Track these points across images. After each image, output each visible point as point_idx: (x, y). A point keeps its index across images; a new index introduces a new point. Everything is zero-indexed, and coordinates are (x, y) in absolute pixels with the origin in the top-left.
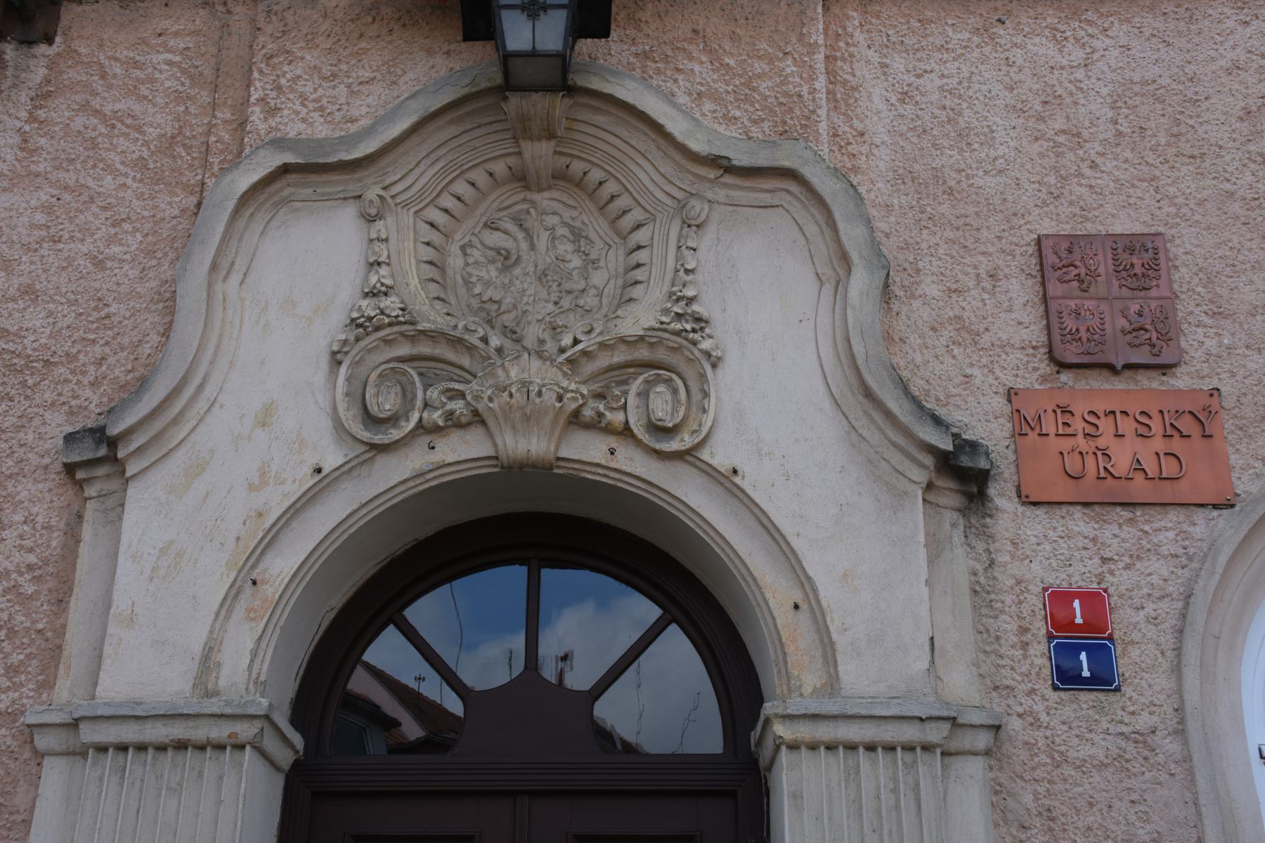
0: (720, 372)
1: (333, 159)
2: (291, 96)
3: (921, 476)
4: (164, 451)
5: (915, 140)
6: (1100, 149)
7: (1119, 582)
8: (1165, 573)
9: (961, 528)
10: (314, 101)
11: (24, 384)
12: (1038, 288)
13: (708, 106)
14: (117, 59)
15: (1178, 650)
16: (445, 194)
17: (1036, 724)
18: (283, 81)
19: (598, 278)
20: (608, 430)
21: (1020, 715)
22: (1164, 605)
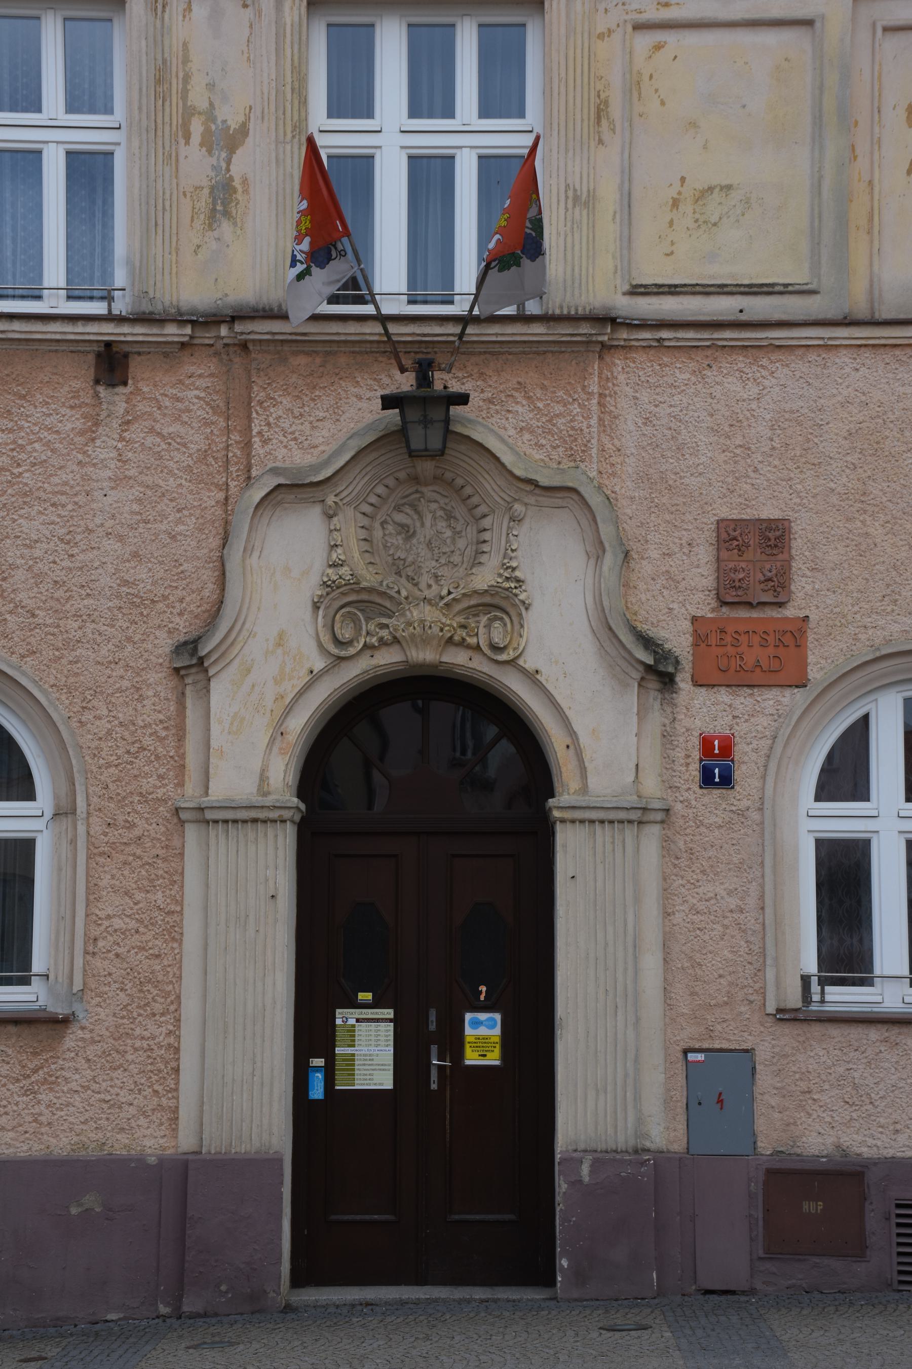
0: (530, 612)
1: (307, 481)
2: (277, 430)
3: (637, 675)
4: (228, 661)
5: (651, 452)
6: (760, 459)
7: (741, 729)
8: (765, 724)
9: (659, 700)
10: (290, 433)
11: (141, 614)
12: (715, 552)
13: (527, 436)
14: (166, 396)
15: (766, 766)
16: (371, 494)
17: (689, 806)
18: (271, 420)
19: (461, 543)
20: (469, 647)
21: (681, 802)
22: (762, 742)
